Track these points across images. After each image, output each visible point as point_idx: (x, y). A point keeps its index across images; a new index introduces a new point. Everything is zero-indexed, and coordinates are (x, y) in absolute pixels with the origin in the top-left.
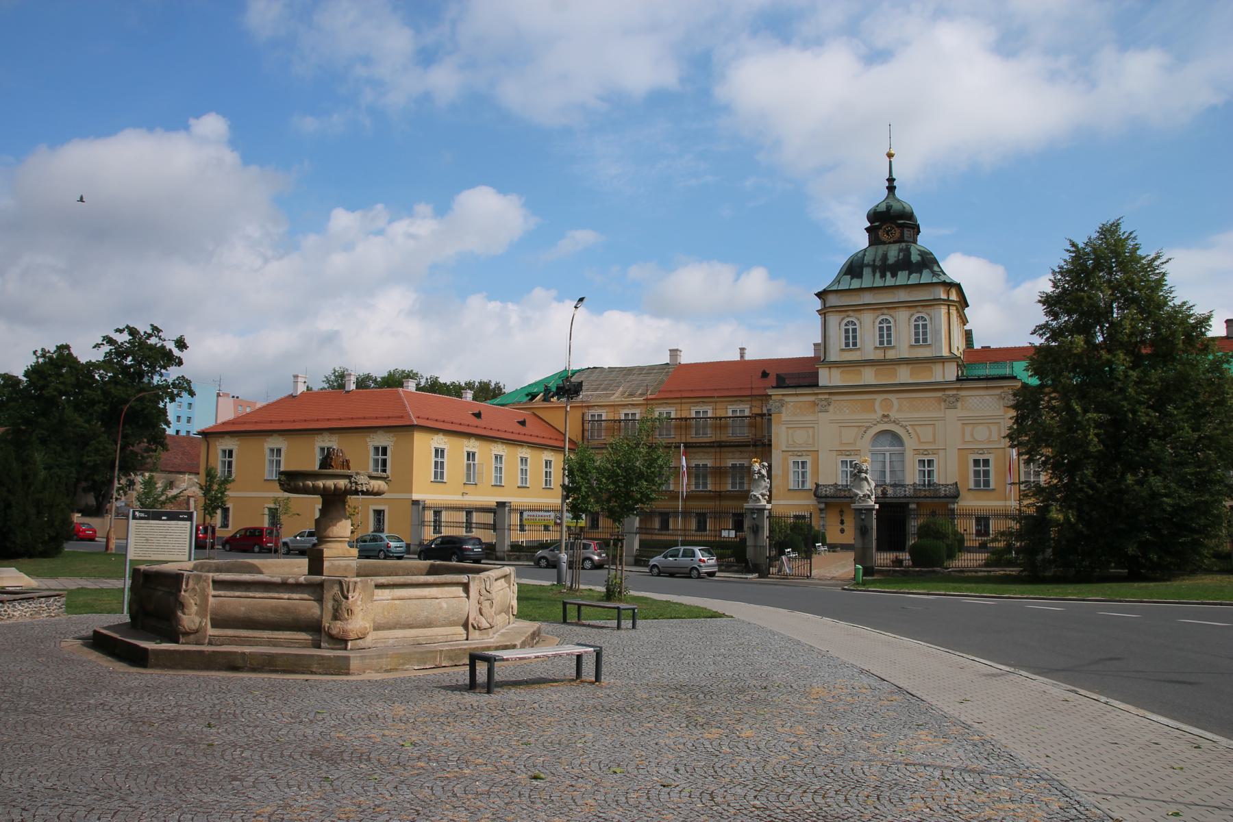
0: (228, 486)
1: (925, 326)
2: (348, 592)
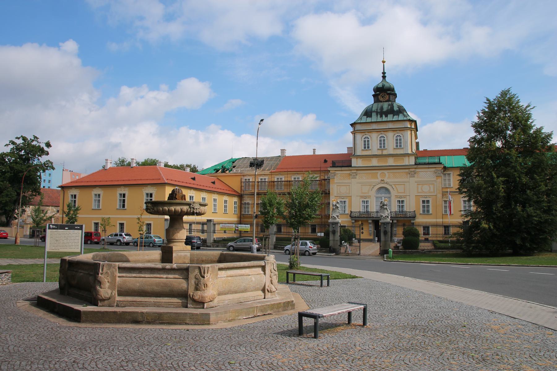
0: (78, 212)
1: (400, 140)
2: (204, 273)
